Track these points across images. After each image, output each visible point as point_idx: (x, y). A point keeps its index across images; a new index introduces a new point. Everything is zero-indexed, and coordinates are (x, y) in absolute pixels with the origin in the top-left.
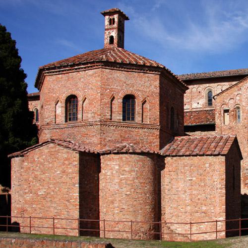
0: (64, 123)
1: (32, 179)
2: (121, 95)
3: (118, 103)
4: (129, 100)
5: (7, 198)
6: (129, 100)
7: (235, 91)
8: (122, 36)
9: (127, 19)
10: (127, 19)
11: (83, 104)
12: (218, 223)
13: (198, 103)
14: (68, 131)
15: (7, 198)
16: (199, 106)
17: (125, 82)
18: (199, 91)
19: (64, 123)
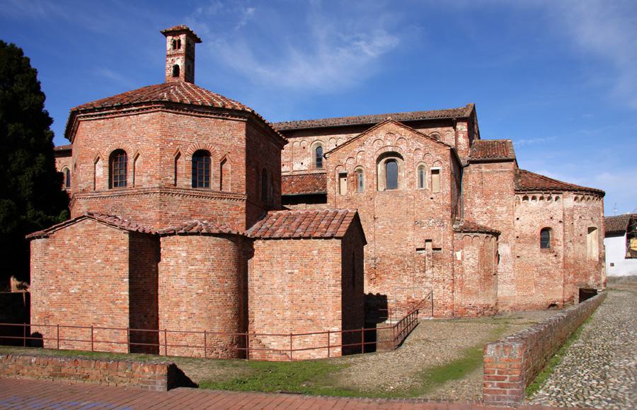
2: (190, 150)
3: (186, 162)
4: (201, 157)
6: (201, 157)
9: (199, 41)
10: (199, 41)
13: (302, 164)
16: (304, 168)
17: (194, 132)
18: (302, 146)
19: (108, 190)
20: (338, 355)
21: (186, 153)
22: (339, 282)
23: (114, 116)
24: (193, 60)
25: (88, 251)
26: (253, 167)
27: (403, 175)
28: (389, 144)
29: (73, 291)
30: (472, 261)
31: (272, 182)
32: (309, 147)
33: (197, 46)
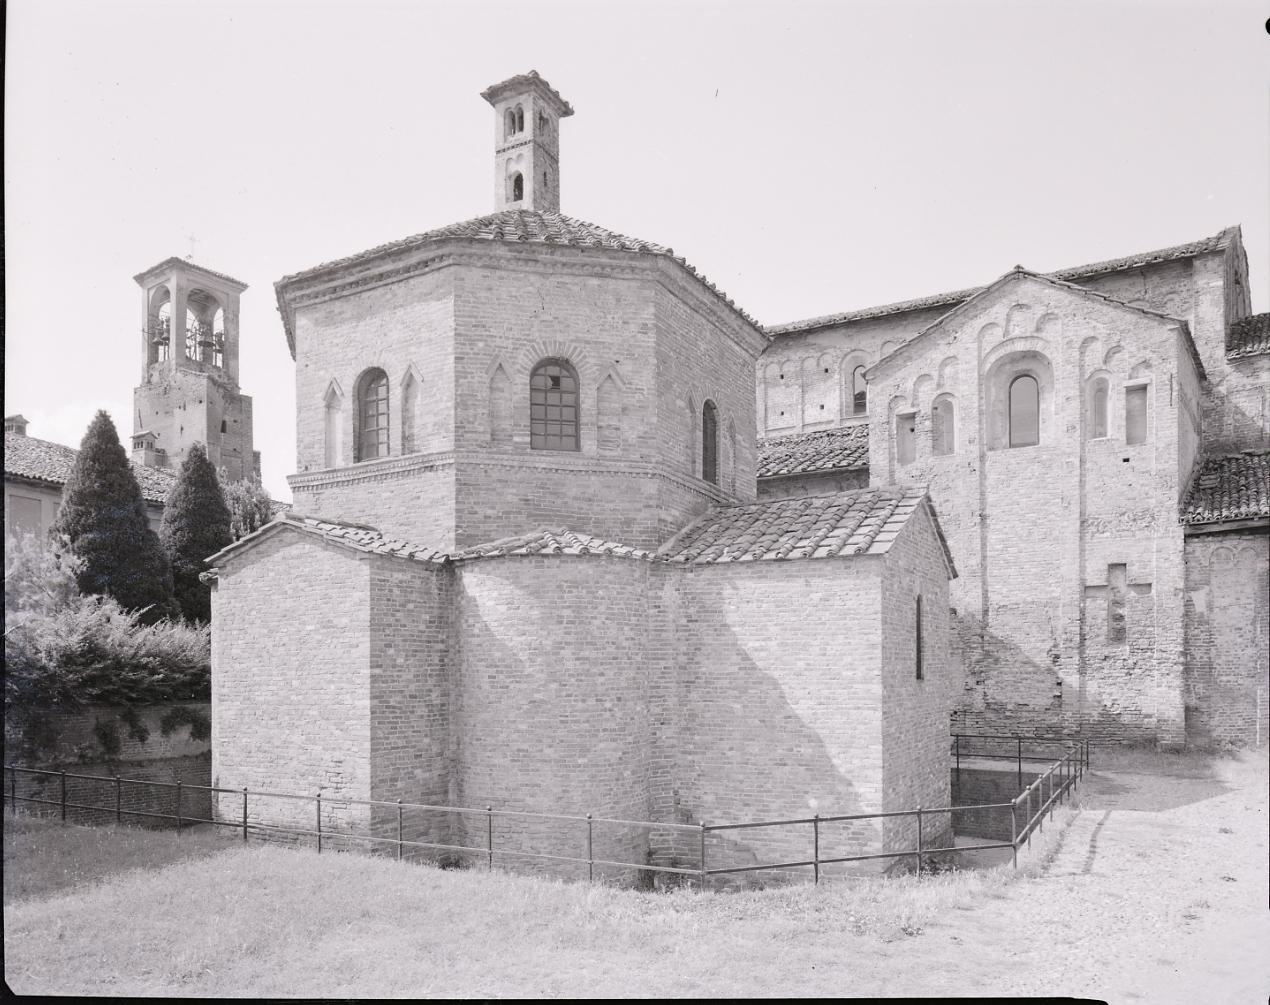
0: (351, 465)
1: (239, 651)
2: (526, 360)
3: (517, 390)
4: (554, 377)
5: (147, 609)
6: (554, 377)
7: (937, 353)
8: (549, 170)
9: (566, 111)
10: (566, 111)
11: (826, 820)
12: (819, 824)
13: (822, 407)
14: (360, 493)
15: (147, 609)
16: (825, 415)
17: (534, 313)
18: (823, 366)
19: (351, 465)
20: (1248, 310)
21: (518, 367)
22: (876, 672)
23: (360, 289)
24: (555, 160)
25: (289, 603)
26: (679, 397)
27: (1053, 408)
28: (1016, 332)
29: (261, 699)
30: (1234, 611)
31: (733, 437)
32: (836, 367)
33: (564, 123)
